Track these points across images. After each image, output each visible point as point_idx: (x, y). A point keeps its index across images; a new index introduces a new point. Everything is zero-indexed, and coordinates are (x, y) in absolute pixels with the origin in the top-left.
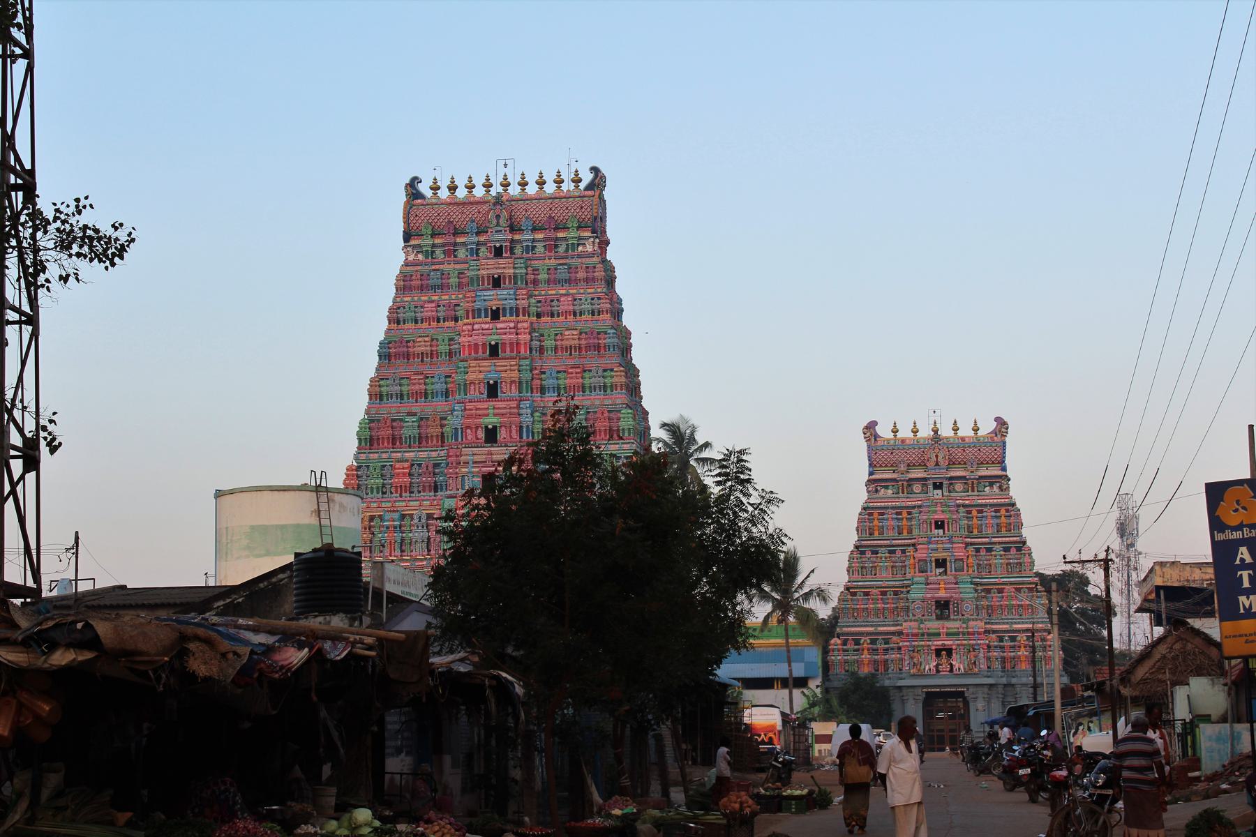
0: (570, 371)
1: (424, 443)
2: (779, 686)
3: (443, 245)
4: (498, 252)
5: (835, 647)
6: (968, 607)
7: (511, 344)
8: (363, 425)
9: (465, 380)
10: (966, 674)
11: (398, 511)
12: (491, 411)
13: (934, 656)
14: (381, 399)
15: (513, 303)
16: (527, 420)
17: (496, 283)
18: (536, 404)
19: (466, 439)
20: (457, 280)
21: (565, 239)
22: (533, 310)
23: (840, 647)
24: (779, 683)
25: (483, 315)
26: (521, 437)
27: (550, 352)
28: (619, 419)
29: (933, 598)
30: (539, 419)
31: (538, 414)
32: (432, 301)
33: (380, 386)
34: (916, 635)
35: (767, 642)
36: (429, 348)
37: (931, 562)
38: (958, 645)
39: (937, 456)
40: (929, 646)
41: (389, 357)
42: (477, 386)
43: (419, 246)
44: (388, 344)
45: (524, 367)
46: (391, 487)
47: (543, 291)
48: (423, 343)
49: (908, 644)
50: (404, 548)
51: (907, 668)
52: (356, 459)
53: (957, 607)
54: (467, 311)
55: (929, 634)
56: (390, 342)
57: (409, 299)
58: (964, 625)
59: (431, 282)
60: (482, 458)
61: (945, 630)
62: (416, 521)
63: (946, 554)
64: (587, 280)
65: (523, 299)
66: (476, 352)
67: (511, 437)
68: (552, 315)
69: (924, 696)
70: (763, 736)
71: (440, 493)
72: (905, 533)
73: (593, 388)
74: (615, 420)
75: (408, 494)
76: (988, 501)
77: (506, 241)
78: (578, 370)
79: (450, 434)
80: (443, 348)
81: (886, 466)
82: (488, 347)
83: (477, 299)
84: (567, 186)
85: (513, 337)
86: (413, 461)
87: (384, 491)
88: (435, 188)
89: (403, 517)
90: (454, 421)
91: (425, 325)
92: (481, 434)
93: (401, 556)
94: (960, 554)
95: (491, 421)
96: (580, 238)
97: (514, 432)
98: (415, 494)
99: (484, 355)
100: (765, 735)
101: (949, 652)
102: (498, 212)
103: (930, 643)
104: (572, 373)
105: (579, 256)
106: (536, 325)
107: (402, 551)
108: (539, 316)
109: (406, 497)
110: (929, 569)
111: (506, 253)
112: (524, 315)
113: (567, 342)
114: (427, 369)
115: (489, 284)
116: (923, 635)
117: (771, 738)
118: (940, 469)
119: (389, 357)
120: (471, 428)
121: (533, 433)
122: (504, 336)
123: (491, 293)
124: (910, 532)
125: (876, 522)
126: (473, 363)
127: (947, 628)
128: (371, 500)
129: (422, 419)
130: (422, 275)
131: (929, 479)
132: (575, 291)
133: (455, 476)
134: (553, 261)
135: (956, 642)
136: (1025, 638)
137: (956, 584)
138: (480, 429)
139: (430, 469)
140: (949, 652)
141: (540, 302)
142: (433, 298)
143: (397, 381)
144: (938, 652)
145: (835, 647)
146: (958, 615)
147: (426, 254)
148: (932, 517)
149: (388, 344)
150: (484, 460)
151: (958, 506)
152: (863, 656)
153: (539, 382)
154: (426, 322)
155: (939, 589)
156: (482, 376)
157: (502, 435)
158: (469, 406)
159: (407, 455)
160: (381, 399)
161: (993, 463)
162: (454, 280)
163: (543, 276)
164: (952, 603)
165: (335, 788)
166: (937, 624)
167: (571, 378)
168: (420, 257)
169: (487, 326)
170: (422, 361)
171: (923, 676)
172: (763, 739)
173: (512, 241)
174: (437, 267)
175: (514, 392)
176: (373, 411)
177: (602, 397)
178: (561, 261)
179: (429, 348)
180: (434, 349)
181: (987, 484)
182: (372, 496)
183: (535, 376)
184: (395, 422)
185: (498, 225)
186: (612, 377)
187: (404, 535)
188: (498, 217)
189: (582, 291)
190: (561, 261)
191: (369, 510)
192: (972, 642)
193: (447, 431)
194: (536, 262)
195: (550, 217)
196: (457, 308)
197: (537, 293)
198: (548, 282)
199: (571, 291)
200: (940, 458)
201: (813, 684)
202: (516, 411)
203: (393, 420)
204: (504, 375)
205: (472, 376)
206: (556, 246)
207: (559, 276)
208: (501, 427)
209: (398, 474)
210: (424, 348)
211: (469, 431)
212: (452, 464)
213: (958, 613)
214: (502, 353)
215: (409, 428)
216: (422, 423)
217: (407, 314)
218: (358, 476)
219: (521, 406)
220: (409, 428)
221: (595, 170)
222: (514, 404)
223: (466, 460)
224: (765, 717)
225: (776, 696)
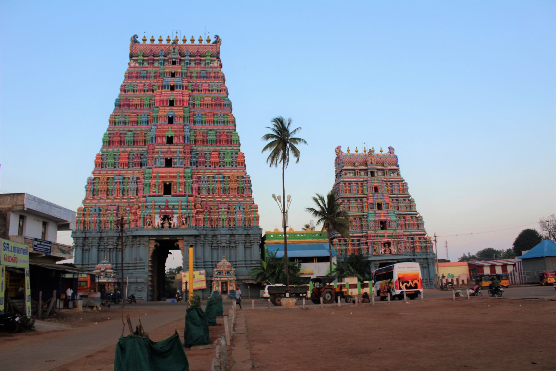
0: (208, 114)
1: (136, 144)
2: (316, 261)
3: (148, 60)
4: (174, 63)
5: (336, 243)
6: (393, 225)
7: (180, 101)
8: (106, 135)
9: (157, 116)
10: (398, 254)
11: (121, 175)
12: (170, 129)
13: (383, 246)
14: (115, 124)
15: (181, 83)
16: (187, 134)
17: (173, 75)
18: (191, 128)
19: (157, 142)
20: (154, 74)
21: (205, 60)
22: (190, 88)
23: (338, 243)
24: (316, 259)
25: (166, 88)
26: (184, 142)
27: (197, 106)
28: (231, 136)
29: (379, 220)
30: (193, 134)
31: (192, 132)
32: (142, 83)
33: (115, 118)
34: (374, 236)
35: (305, 240)
36: (140, 102)
37: (375, 204)
38: (393, 241)
39: (371, 160)
40: (381, 241)
41: (120, 106)
42: (163, 118)
43: (137, 60)
44: (115, 116)
45: (186, 111)
46: (118, 164)
47: (194, 80)
48: (137, 100)
49: (371, 241)
50: (124, 193)
51: (371, 252)
52: (101, 151)
53: (390, 224)
54: (159, 87)
55: (380, 236)
56: (121, 100)
57: (131, 82)
58: (395, 232)
59: (142, 75)
60: (166, 150)
61: (387, 234)
62: (131, 180)
63: (381, 201)
64: (215, 77)
65: (186, 82)
66: (163, 103)
67: (180, 141)
68: (199, 91)
69: (379, 265)
70: (410, 282)
71: (143, 167)
72: (360, 192)
73: (218, 122)
74: (229, 137)
75: (127, 167)
76: (394, 179)
77: (178, 59)
78: (212, 114)
79: (149, 140)
80: (146, 102)
81: (349, 164)
82: (169, 102)
83: (164, 81)
84: (204, 42)
85: (181, 97)
86: (130, 152)
87: (115, 166)
88: (145, 40)
89: (124, 178)
90: (152, 134)
91: (138, 93)
92: (165, 140)
93: (123, 197)
94: (387, 201)
95: (170, 134)
96: (211, 60)
97: (181, 139)
98: (131, 168)
99: (167, 105)
100: (412, 282)
101: (389, 244)
102: (174, 47)
103: (381, 240)
104: (209, 115)
105: (211, 67)
106: (191, 94)
107: (123, 195)
108: (192, 91)
109: (126, 169)
110: (374, 208)
111: (178, 64)
112: (186, 89)
113: (206, 102)
114: (138, 111)
115: (169, 76)
116: (377, 236)
117: (416, 284)
118: (373, 165)
119: (120, 106)
120: (160, 137)
121: (190, 141)
122: (176, 97)
123: (171, 79)
124: (362, 192)
125: (347, 187)
126: (162, 108)
127: (388, 233)
128: (108, 170)
129: (135, 134)
130: (137, 72)
131: (369, 169)
132: (209, 82)
133: (151, 158)
134: (199, 69)
135: (393, 240)
136: (418, 238)
137: (388, 214)
138: (164, 137)
139: (139, 155)
140: (389, 244)
141: (192, 85)
142: (142, 82)
143: (124, 116)
144: (384, 244)
145: (336, 243)
146: (390, 228)
147: (140, 63)
148: (373, 185)
149: (115, 116)
150: (166, 151)
151: (383, 181)
152: (349, 247)
153: (193, 118)
154: (134, 106)
155: (381, 216)
156: (165, 114)
157: (175, 140)
158: (159, 127)
159: (127, 149)
160: (115, 124)
161: (393, 164)
162: (152, 75)
163: (194, 75)
164: (387, 222)
165: (62, 295)
166: (383, 231)
167: (209, 117)
168: (137, 65)
169: (168, 93)
170: (136, 108)
171: (379, 255)
172: (411, 285)
173: (180, 60)
174: (145, 69)
175: (181, 121)
176: (111, 129)
177: (223, 126)
178: (203, 69)
179: (140, 102)
180: (142, 103)
181: (391, 173)
182: (109, 168)
183: (191, 116)
184: (121, 135)
185: (174, 52)
186: (227, 118)
187: (125, 187)
188: (174, 49)
189: (212, 82)
190: (203, 69)
191: (107, 174)
192: (399, 239)
193: (148, 138)
194: (191, 69)
195: (198, 51)
196: (153, 86)
197: (191, 81)
198: (197, 77)
199: (207, 82)
200: (373, 160)
201: (216, 273)
202: (182, 129)
203: (121, 134)
204: (176, 114)
205: (160, 114)
206: (200, 64)
207: (202, 75)
208: (174, 137)
209: (122, 158)
210: (137, 102)
211: (159, 138)
212: (150, 153)
213: (390, 226)
214: (175, 104)
215: (129, 137)
216: (135, 135)
217: (130, 88)
218: (102, 159)
219: (185, 128)
220: (129, 137)
221: (217, 37)
222: (182, 127)
223: (158, 151)
224: (410, 269)
225: (315, 266)
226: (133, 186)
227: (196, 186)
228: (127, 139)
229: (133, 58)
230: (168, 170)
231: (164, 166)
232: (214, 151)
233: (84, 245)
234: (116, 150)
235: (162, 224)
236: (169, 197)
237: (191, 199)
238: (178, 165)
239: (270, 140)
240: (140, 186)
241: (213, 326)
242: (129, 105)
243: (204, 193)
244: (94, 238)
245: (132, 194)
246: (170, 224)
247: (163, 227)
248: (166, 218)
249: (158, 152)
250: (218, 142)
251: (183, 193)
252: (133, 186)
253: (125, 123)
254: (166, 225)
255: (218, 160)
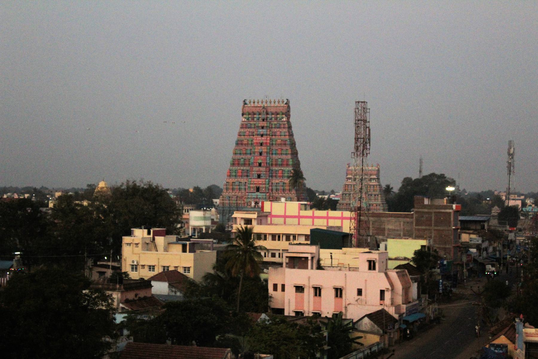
17: (263, 128)
92: (258, 164)
95: (260, 161)
114: (246, 148)
156: (258, 150)
157: (262, 164)
163: (273, 126)
175: (265, 154)
188: (264, 111)
226: (243, 187)
227: (270, 188)
228: (241, 163)
229: (245, 116)
230: (259, 180)
231: (257, 178)
232: (280, 170)
233: (223, 213)
234: (236, 168)
235: (255, 206)
236: (258, 193)
237: (268, 194)
238: (263, 178)
239: (291, 178)
240: (247, 187)
241: (305, 300)
242: (242, 144)
243: (274, 191)
244: (227, 210)
245: (243, 191)
246: (258, 206)
247: (255, 207)
248: (256, 203)
249: (254, 171)
250: (282, 165)
251: (264, 192)
252: (243, 187)
253: (240, 154)
254: (257, 206)
255: (281, 175)
